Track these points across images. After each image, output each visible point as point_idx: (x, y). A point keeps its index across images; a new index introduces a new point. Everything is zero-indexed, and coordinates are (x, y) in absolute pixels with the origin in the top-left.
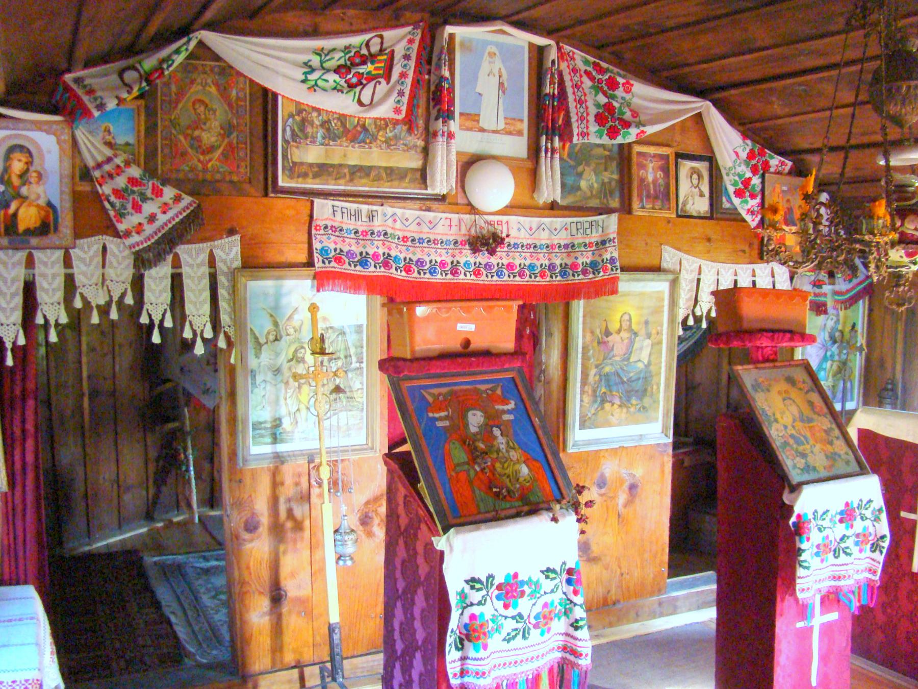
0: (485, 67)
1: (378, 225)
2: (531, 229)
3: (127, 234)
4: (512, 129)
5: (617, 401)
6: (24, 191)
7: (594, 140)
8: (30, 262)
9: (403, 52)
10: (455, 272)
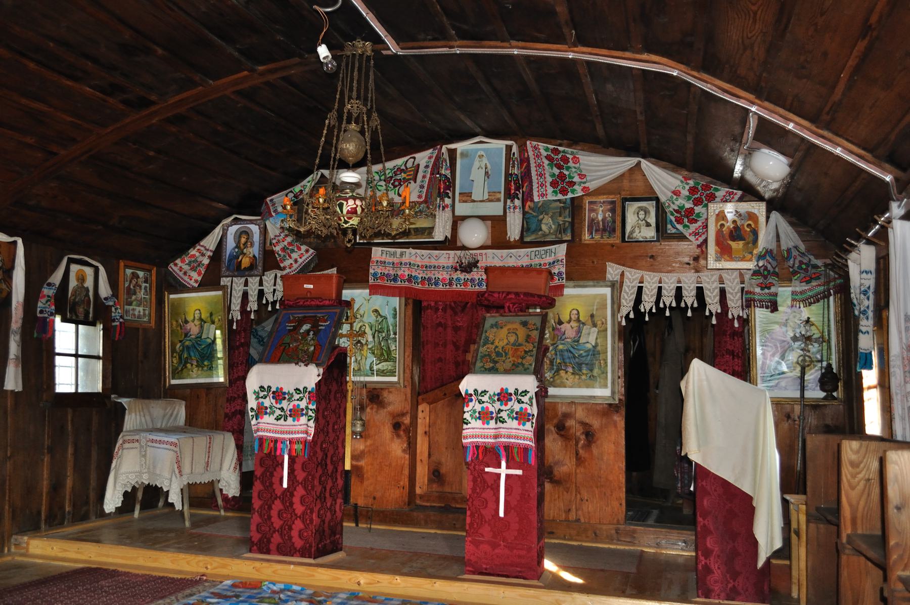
0: (477, 164)
1: (405, 259)
2: (502, 257)
3: (284, 268)
4: (493, 198)
5: (570, 370)
6: (245, 251)
7: (551, 197)
8: (246, 284)
9: (425, 164)
10: (451, 284)
